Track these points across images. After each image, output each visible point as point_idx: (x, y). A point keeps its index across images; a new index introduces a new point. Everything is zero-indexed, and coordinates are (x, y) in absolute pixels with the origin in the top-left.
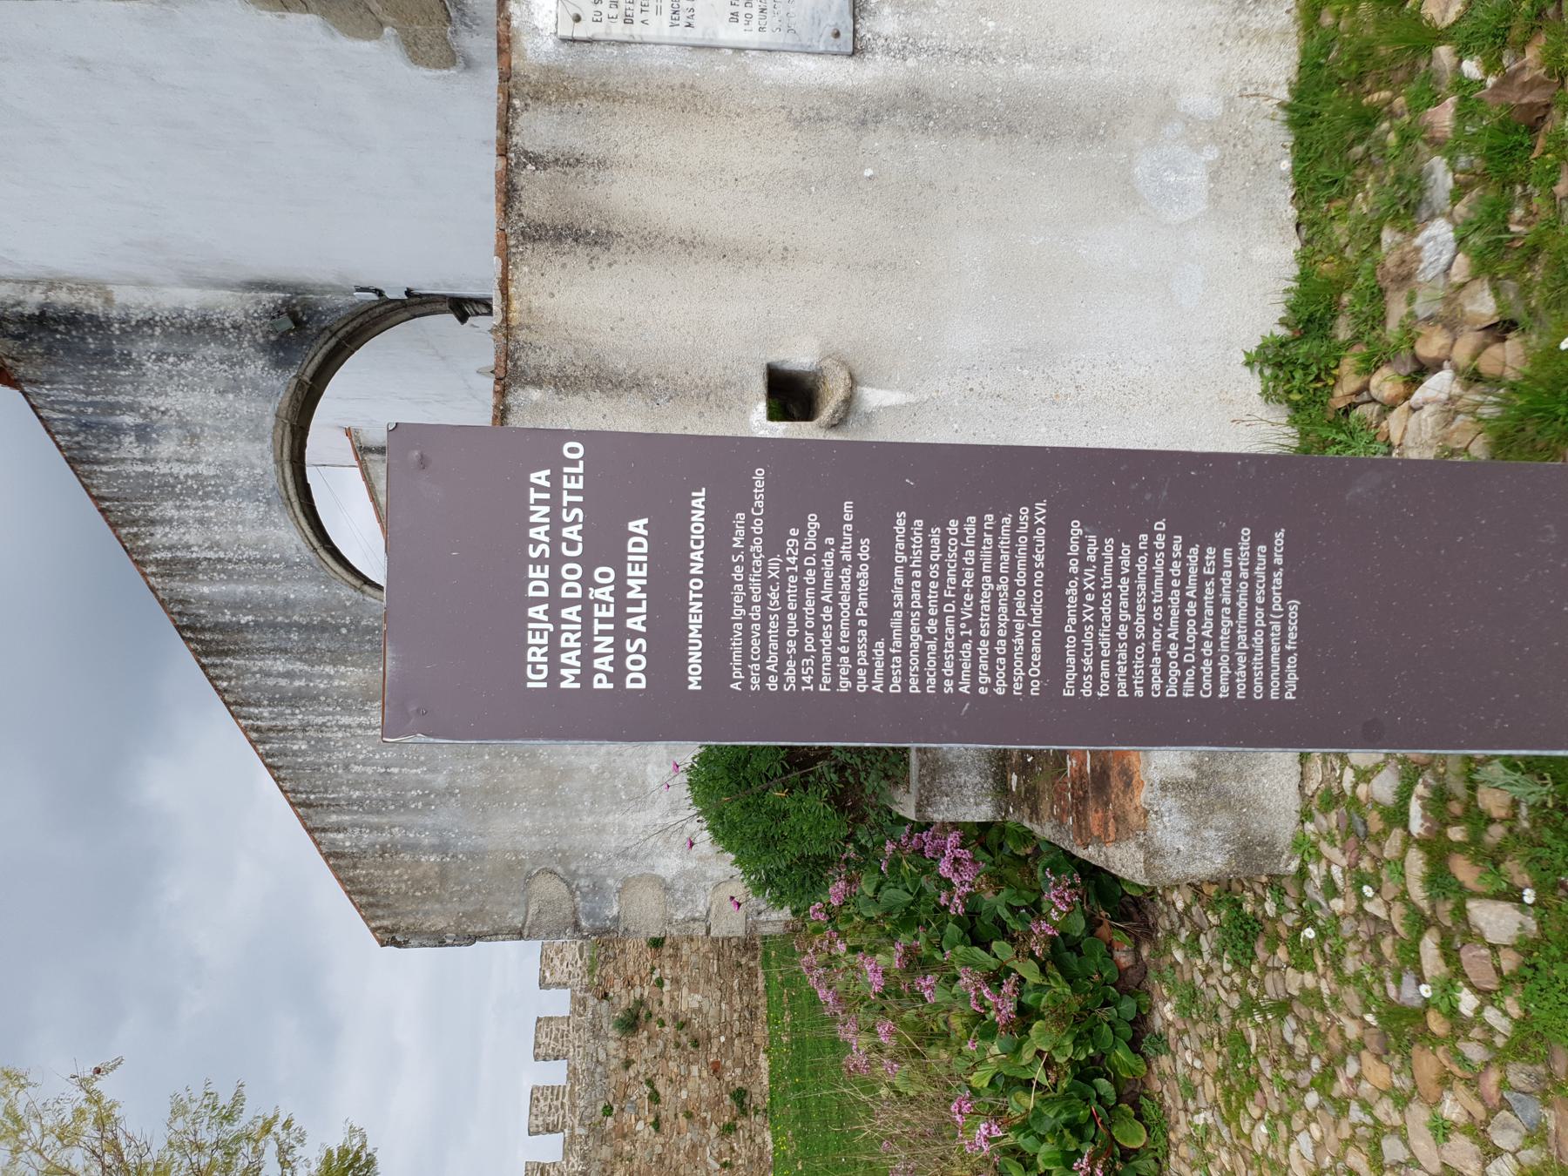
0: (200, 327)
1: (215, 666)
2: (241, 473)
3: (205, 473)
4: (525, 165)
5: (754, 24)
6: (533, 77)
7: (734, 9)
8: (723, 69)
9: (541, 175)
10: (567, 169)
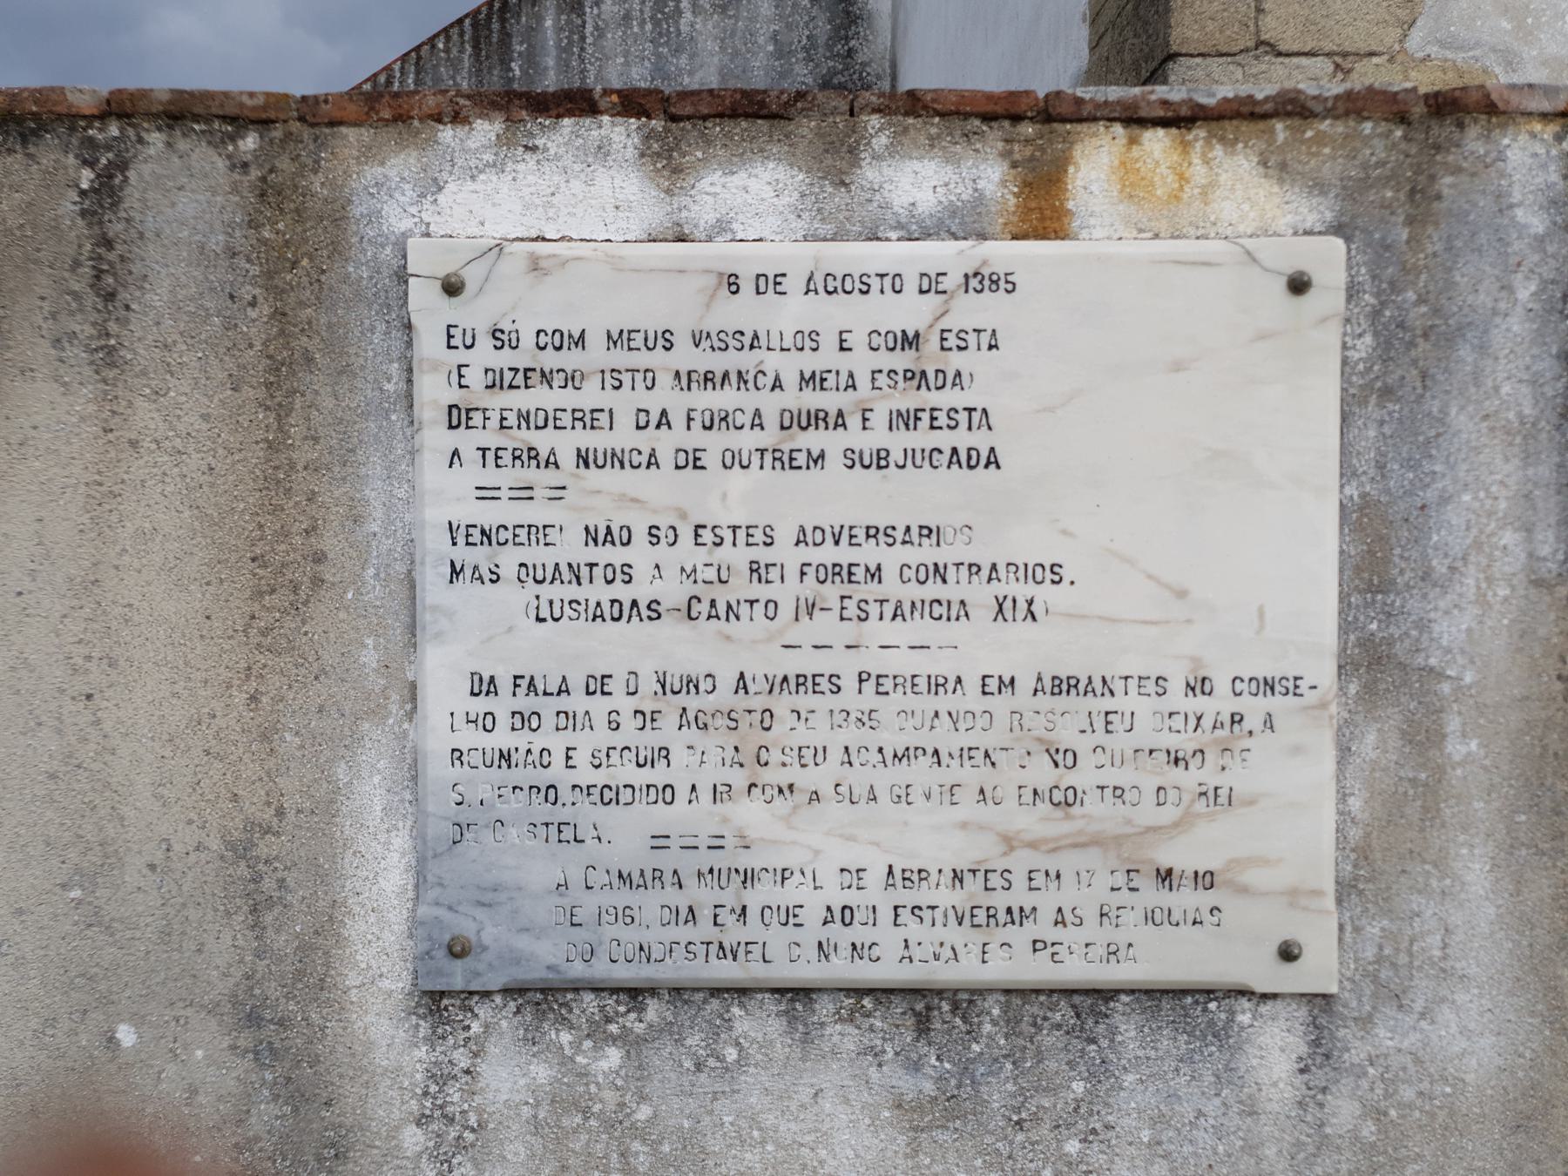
0: (848, 13)
1: (462, 34)
2: (683, 60)
3: (683, 21)
4: (90, 164)
5: (469, 738)
6: (316, 183)
7: (505, 685)
8: (370, 657)
9: (69, 205)
10: (87, 270)
